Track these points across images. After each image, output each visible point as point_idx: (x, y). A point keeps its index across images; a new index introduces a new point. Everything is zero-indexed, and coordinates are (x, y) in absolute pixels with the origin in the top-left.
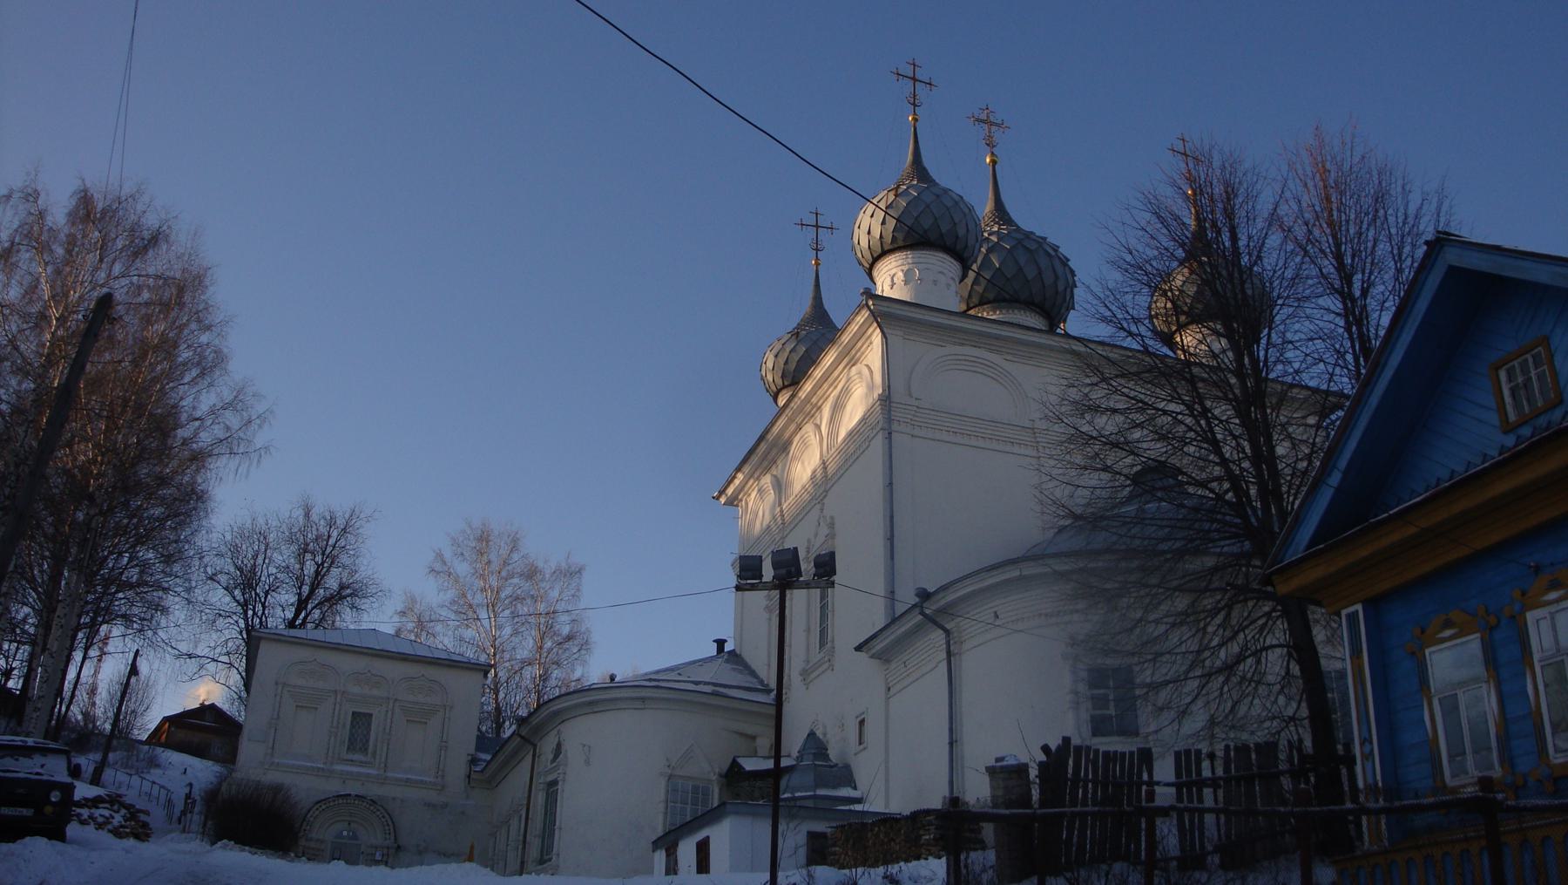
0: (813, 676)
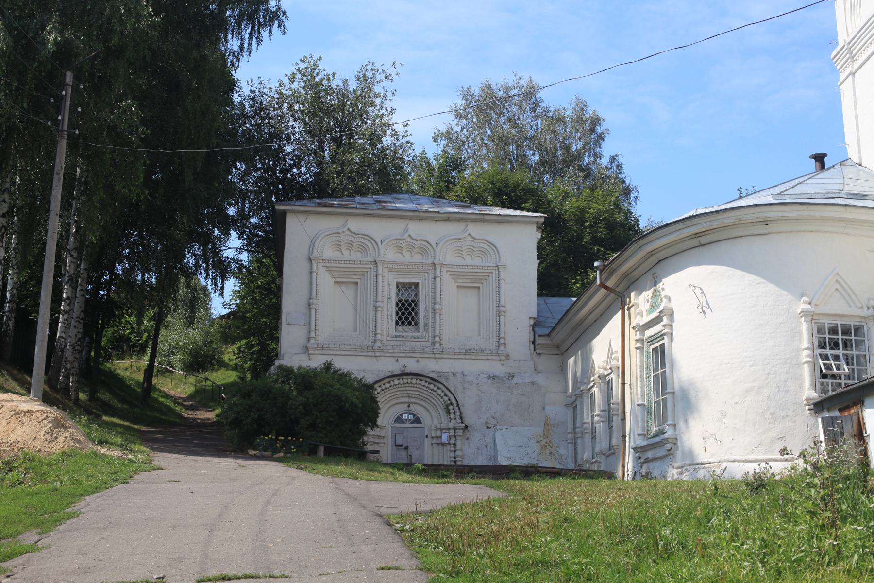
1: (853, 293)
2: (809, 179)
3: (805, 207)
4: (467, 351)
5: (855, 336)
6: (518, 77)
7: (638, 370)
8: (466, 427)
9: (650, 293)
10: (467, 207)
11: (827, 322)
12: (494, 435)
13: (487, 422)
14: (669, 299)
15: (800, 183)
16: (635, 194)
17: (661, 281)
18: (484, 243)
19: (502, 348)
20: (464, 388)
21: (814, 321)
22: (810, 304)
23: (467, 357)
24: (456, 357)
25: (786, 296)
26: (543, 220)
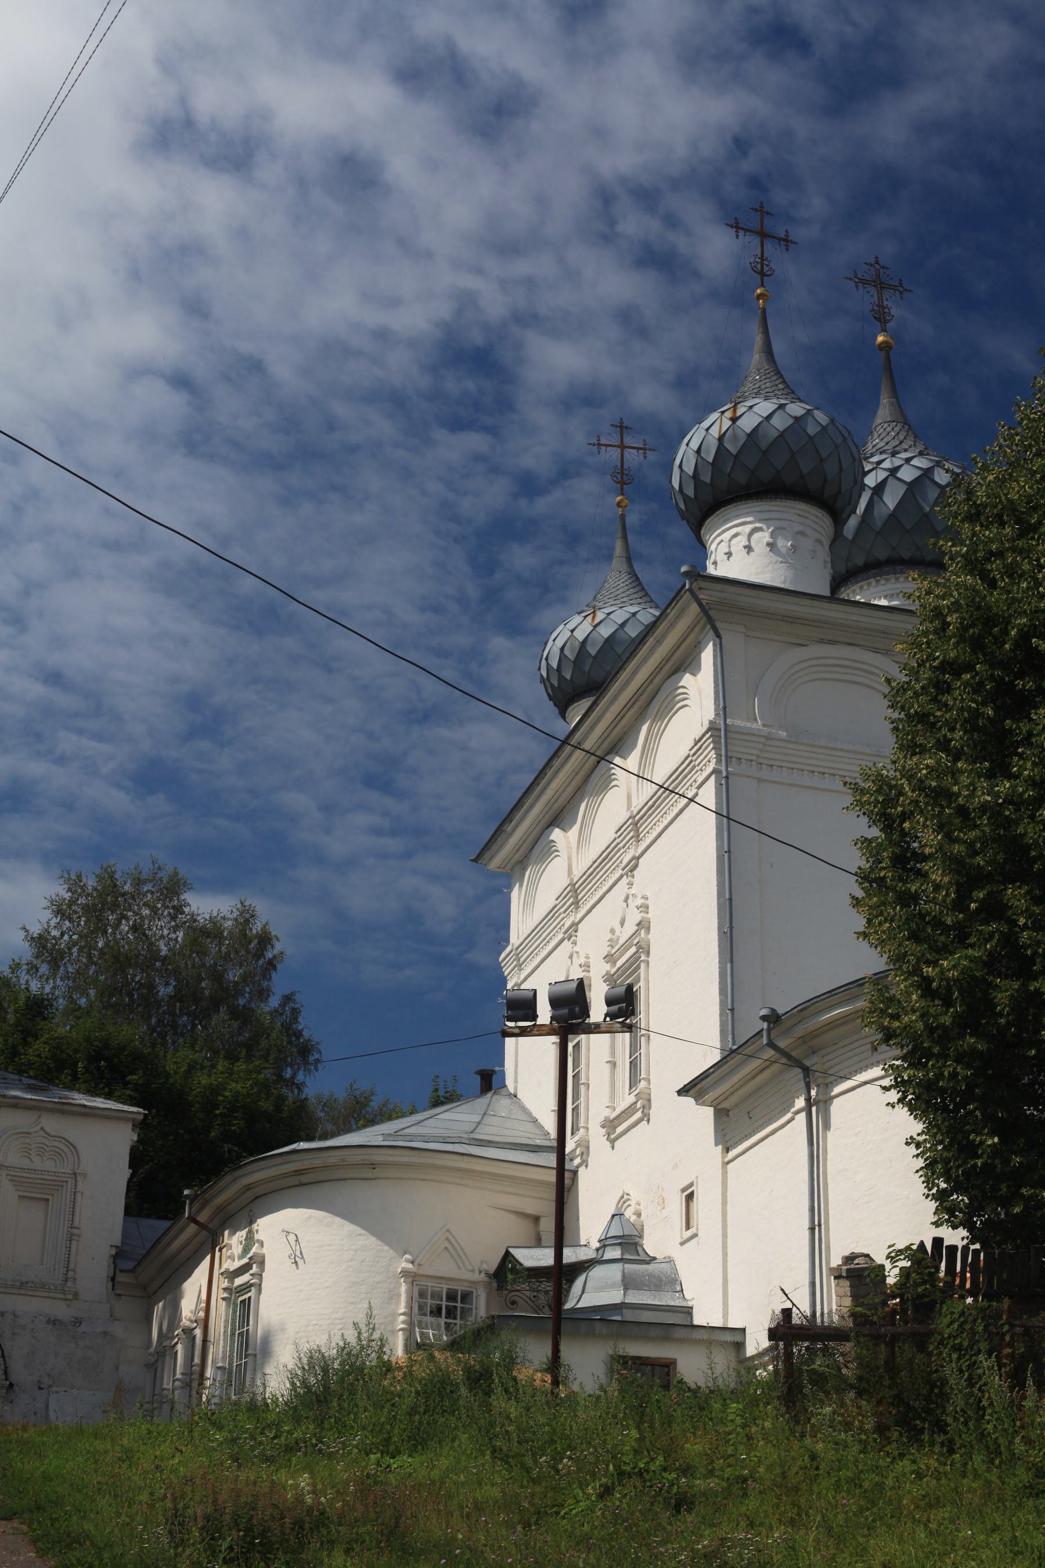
0: (619, 1130)
1: (464, 1253)
2: (445, 1111)
3: (416, 1153)
4: (23, 1285)
5: (462, 1302)
6: (156, 866)
7: (222, 1325)
8: (11, 1385)
9: (242, 1234)
10: (43, 1090)
11: (430, 1284)
12: (48, 1398)
13: (39, 1381)
14: (262, 1244)
15: (431, 1117)
16: (316, 1056)
17: (256, 1221)
18: (61, 1142)
19: (70, 1283)
20: (14, 1334)
21: (415, 1283)
22: (412, 1263)
23: (22, 1292)
24: (7, 1290)
25: (387, 1251)
26: (142, 1117)
